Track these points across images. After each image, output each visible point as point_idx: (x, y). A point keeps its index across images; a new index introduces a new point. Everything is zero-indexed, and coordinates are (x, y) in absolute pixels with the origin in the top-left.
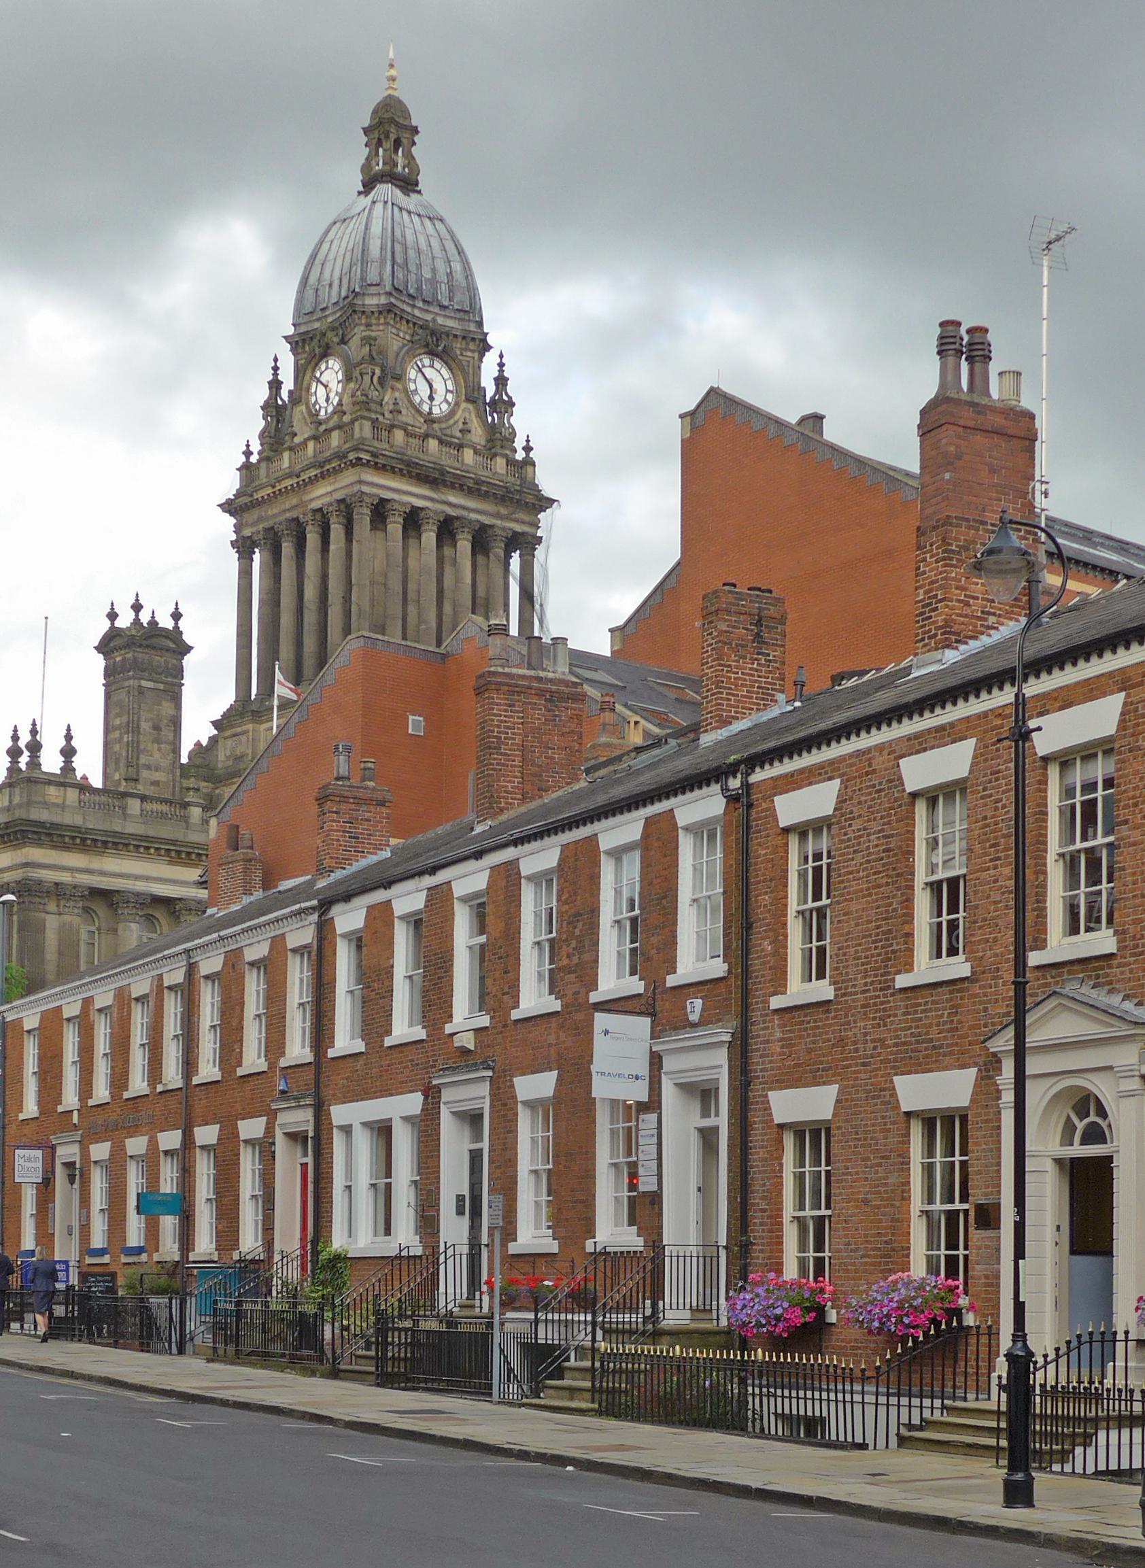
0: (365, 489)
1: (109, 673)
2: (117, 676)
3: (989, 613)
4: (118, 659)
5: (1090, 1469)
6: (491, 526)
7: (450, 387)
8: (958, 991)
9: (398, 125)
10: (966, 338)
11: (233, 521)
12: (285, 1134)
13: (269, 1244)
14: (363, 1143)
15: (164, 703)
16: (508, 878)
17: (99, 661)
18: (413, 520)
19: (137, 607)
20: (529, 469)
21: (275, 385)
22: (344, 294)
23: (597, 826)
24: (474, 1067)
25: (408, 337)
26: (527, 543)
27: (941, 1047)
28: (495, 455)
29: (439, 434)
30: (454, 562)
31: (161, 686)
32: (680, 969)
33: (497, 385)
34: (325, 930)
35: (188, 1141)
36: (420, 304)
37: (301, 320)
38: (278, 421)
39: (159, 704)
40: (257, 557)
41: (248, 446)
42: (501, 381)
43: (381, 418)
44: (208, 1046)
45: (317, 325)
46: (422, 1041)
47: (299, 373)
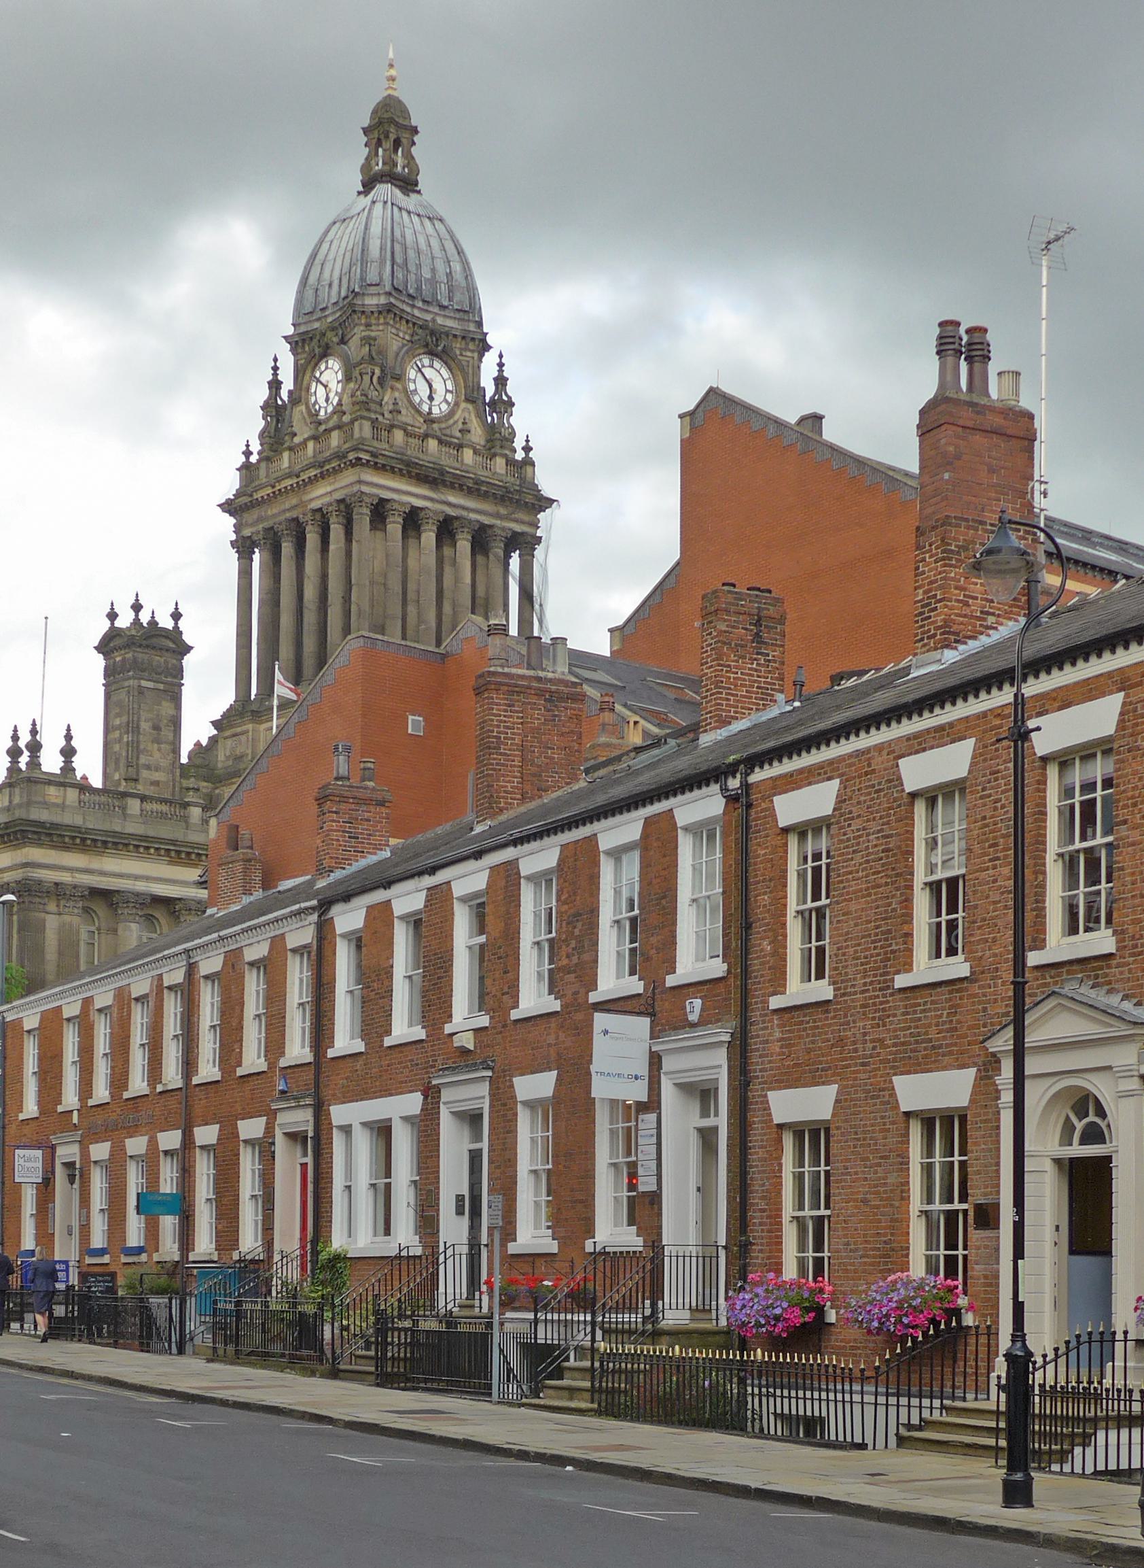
0: (365, 489)
1: (109, 673)
2: (117, 676)
3: (988, 613)
4: (118, 659)
5: (1089, 1469)
6: (491, 526)
7: (450, 387)
8: (958, 991)
9: (397, 125)
10: (965, 338)
11: (233, 521)
12: (285, 1134)
13: (268, 1244)
14: (363, 1143)
15: (164, 703)
16: (507, 878)
17: (99, 661)
18: (413, 520)
19: (137, 607)
20: (529, 469)
21: (275, 385)
22: (343, 294)
23: (596, 826)
24: (473, 1067)
25: (407, 337)
26: (526, 543)
27: (940, 1047)
28: (494, 455)
29: (439, 434)
30: (454, 562)
31: (161, 686)
32: (680, 969)
33: (496, 385)
34: (324, 930)
35: (188, 1141)
36: (420, 304)
37: (301, 320)
38: (278, 421)
39: (159, 704)
40: (256, 557)
41: (248, 446)
42: (501, 381)
43: (380, 418)
44: (208, 1046)
45: (316, 325)
46: (422, 1041)
47: (299, 373)
